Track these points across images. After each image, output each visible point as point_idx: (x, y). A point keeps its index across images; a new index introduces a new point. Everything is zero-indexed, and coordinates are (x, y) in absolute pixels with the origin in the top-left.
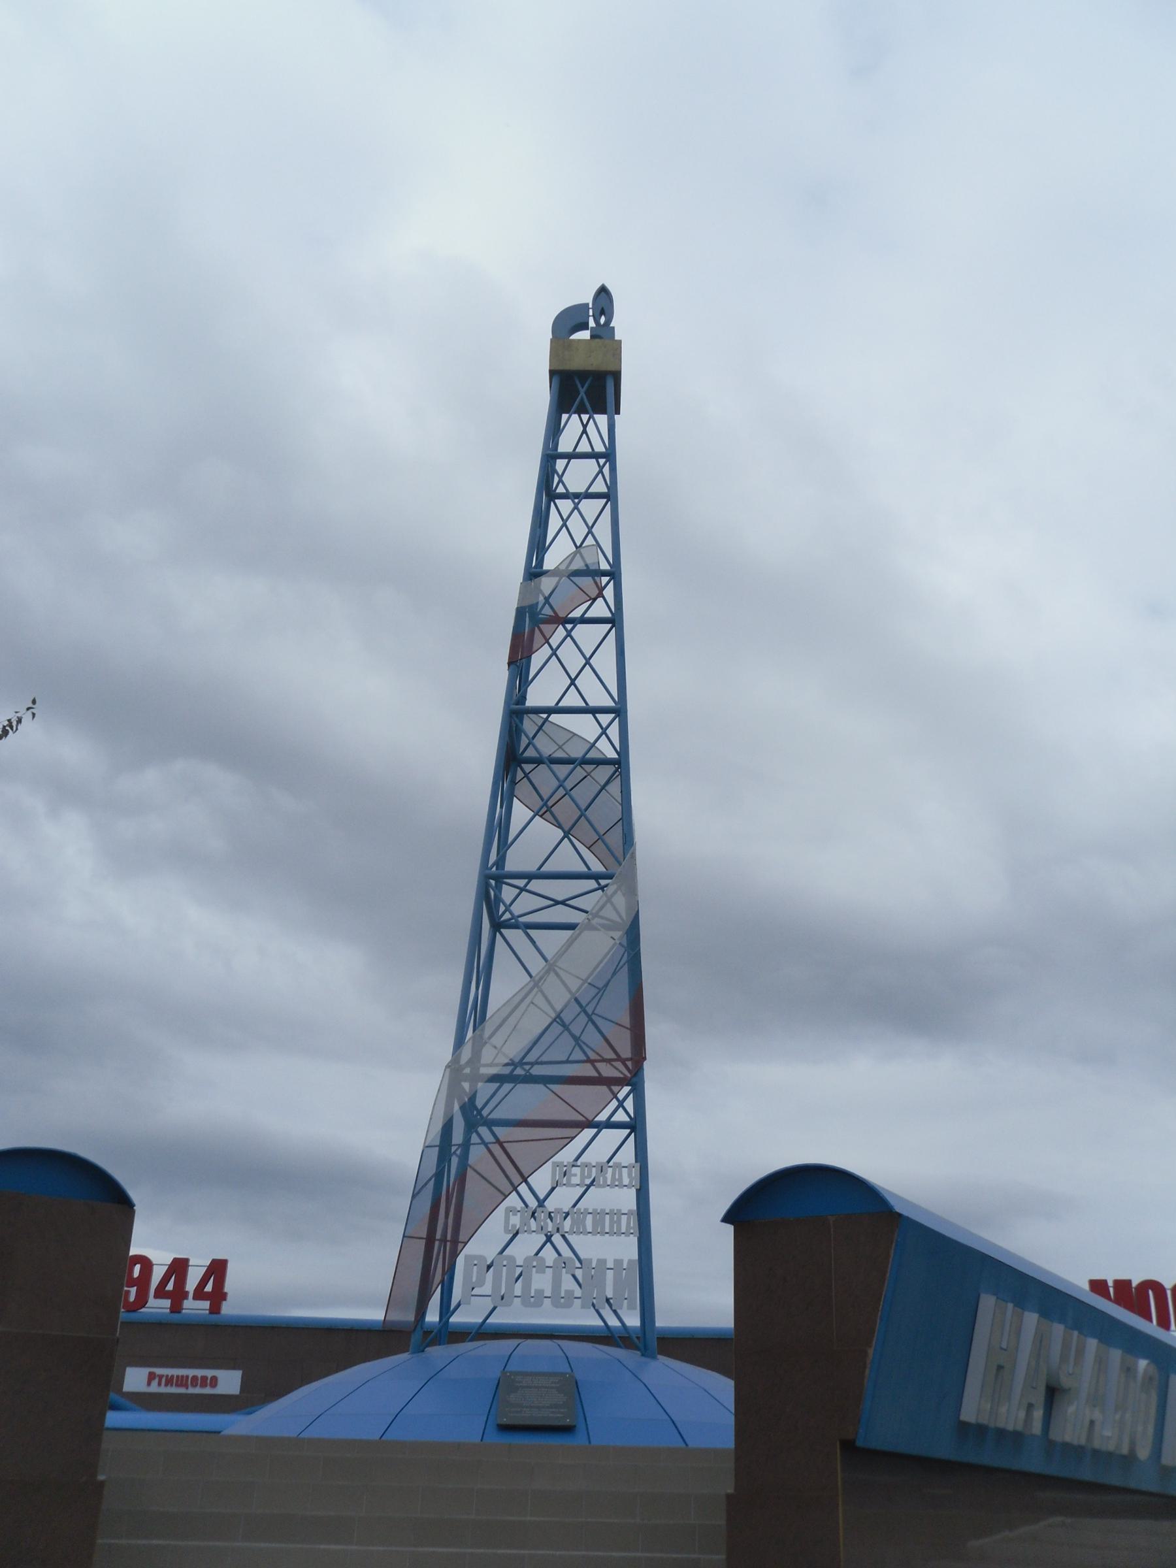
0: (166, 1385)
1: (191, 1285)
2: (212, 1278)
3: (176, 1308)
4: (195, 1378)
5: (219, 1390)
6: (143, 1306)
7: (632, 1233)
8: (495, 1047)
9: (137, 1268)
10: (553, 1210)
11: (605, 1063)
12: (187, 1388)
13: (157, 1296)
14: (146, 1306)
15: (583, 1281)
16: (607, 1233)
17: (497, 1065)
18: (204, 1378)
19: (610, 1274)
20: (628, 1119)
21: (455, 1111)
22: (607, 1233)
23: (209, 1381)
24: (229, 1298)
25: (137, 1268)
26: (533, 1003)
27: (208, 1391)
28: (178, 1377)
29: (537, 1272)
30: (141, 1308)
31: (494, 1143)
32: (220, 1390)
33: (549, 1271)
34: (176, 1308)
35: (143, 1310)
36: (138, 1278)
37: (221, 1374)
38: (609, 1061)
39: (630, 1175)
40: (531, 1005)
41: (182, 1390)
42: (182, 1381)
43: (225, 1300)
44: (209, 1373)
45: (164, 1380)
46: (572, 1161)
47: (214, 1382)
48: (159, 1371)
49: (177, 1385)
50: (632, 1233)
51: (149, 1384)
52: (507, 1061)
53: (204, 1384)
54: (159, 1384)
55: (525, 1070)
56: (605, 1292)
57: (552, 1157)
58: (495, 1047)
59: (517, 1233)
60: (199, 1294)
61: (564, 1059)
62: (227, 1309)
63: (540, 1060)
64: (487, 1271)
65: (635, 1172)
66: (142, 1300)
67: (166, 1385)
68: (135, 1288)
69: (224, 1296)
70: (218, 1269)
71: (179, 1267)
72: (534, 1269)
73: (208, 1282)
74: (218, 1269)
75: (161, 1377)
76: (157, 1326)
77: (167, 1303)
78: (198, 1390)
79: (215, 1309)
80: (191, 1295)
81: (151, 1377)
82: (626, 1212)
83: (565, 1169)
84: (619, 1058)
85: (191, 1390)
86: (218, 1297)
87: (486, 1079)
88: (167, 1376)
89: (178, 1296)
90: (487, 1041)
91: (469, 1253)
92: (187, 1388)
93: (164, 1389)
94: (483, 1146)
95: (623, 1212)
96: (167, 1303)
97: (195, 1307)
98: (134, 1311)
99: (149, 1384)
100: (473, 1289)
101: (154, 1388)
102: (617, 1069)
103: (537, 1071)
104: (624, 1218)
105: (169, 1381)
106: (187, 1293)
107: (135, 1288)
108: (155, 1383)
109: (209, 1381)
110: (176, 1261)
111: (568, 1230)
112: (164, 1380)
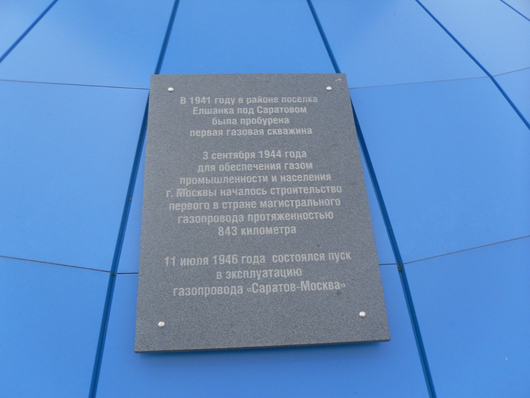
54: (196, 109)
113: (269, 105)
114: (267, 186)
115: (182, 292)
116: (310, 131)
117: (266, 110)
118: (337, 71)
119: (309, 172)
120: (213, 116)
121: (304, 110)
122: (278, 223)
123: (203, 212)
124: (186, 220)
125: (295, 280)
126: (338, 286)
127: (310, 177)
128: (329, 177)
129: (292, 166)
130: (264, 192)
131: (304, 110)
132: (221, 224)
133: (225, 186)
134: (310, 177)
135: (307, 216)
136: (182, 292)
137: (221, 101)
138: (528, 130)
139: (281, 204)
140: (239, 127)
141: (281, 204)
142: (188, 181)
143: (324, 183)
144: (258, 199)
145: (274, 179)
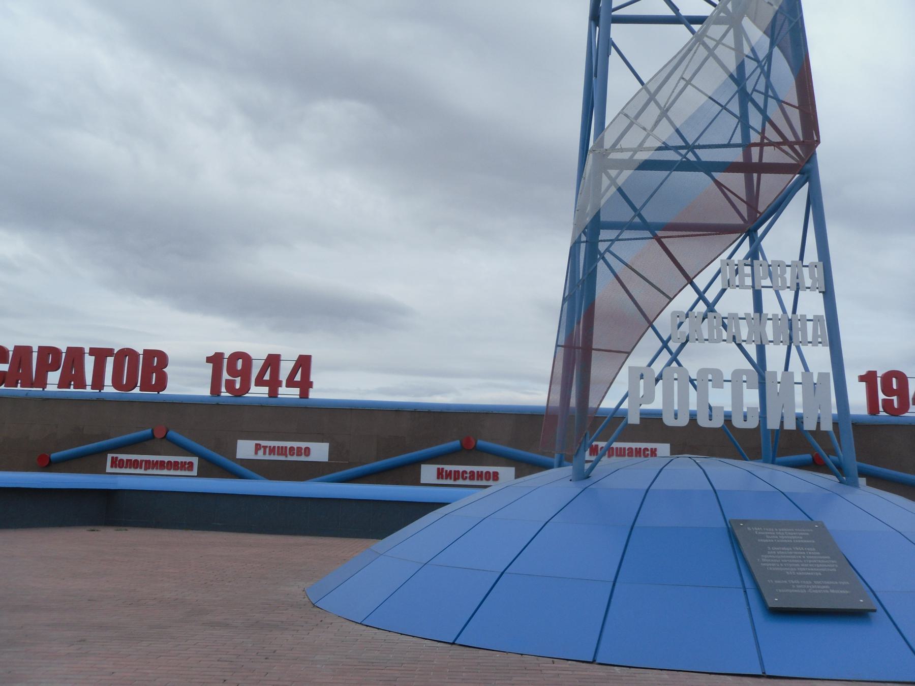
0: (270, 454)
1: (284, 375)
2: (301, 368)
3: (273, 393)
4: (292, 448)
5: (311, 458)
6: (247, 393)
7: (820, 343)
8: (644, 129)
9: (240, 361)
10: (726, 316)
11: (773, 147)
12: (286, 456)
13: (256, 385)
14: (249, 392)
15: (689, 384)
16: (810, 342)
17: (649, 149)
18: (299, 449)
19: (798, 389)
20: (742, 222)
21: (601, 206)
22: (810, 342)
23: (303, 451)
24: (314, 386)
25: (240, 361)
26: (683, 78)
27: (303, 458)
28: (278, 447)
29: (713, 387)
30: (246, 394)
31: (651, 238)
32: (313, 457)
33: (728, 386)
34: (273, 393)
35: (247, 395)
36: (239, 388)
37: (313, 446)
38: (777, 145)
39: (812, 276)
40: (682, 80)
41: (282, 458)
42: (282, 451)
43: (311, 387)
44: (303, 445)
45: (267, 450)
46: (742, 259)
47: (307, 451)
48: (263, 443)
49: (278, 454)
50: (820, 343)
51: (256, 453)
52: (659, 144)
53: (299, 454)
54: (265, 453)
55: (680, 154)
56: (698, 394)
57: (720, 255)
58: (644, 129)
59: (687, 341)
60: (291, 383)
61: (726, 142)
62: (313, 394)
63: (697, 144)
64: (656, 384)
65: (818, 273)
66: (246, 387)
67: (270, 454)
68: (240, 378)
69: (310, 385)
70: (304, 363)
71: (273, 361)
72: (745, 384)
73: (297, 372)
74: (304, 363)
75: (265, 447)
76: (258, 406)
77: (265, 390)
78: (295, 458)
79: (304, 394)
80: (284, 383)
81: (258, 447)
82: (812, 318)
83: (736, 267)
84: (785, 141)
85: (290, 458)
86: (305, 385)
87: (636, 166)
88: (270, 447)
89: (274, 385)
90: (634, 121)
91: (631, 365)
92: (286, 456)
93: (268, 457)
94: (654, 241)
95: (808, 318)
96: (265, 390)
97: (288, 393)
98: (240, 396)
99: (256, 453)
100: (641, 405)
101: (261, 456)
102: (787, 153)
103: (706, 156)
104: (810, 325)
105: (272, 450)
106: (281, 382)
107: (240, 378)
108: (261, 452)
109: (303, 451)
110: (270, 356)
111: (745, 339)
112: (267, 450)
113: (790, 532)
114: (802, 559)
115: (780, 591)
116: (814, 542)
117: (789, 533)
118: (812, 520)
119: (819, 555)
120: (802, 539)
121: (808, 534)
122: (811, 571)
123: (777, 567)
124: (771, 569)
125: (828, 589)
126: (847, 592)
127: (818, 557)
128: (829, 557)
129: (810, 553)
130: (801, 561)
131: (808, 534)
132: (787, 571)
133: (783, 559)
134: (818, 557)
135: (824, 570)
136: (780, 591)
137: (767, 529)
138: (640, 1)
139: (810, 565)
140: (779, 539)
141: (810, 565)
142: (766, 556)
143: (827, 559)
144: (800, 563)
145: (804, 557)
